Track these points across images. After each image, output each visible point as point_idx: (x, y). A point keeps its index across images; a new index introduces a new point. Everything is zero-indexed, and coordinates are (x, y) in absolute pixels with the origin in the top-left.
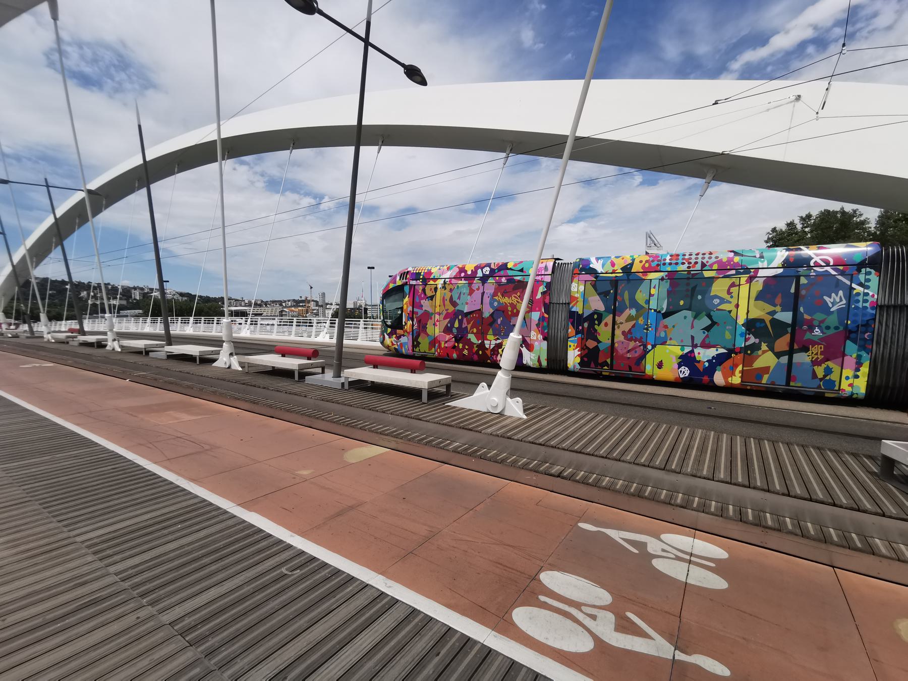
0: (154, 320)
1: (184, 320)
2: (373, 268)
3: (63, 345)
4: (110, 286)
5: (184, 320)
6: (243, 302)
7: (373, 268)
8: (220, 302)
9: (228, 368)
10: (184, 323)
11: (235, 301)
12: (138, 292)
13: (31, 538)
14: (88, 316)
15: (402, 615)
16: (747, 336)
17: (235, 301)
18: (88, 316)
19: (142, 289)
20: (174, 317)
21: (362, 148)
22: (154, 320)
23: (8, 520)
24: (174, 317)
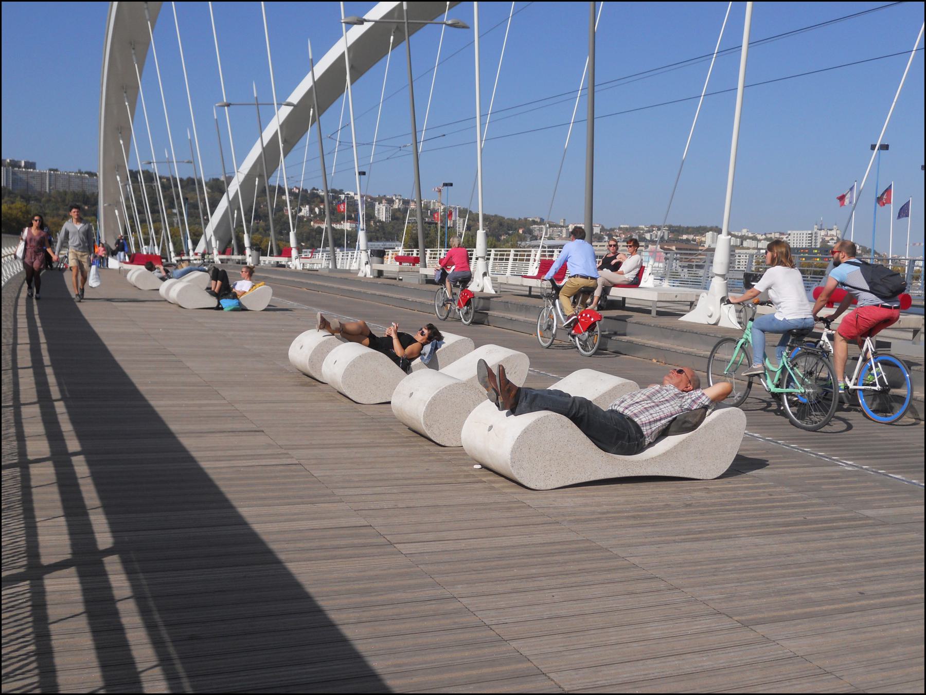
0: (501, 255)
1: (520, 256)
2: (451, 185)
3: (394, 280)
4: (344, 196)
5: (520, 256)
6: (564, 230)
7: (451, 185)
8: (520, 228)
9: (714, 324)
10: (520, 260)
11: (550, 226)
12: (384, 208)
13: (851, 448)
14: (321, 249)
15: (629, 400)
16: (458, 284)
17: (550, 226)
18: (321, 249)
19: (390, 202)
20: (439, 249)
21: (73, 570)
22: (501, 255)
23: (909, 455)
24: (439, 249)
